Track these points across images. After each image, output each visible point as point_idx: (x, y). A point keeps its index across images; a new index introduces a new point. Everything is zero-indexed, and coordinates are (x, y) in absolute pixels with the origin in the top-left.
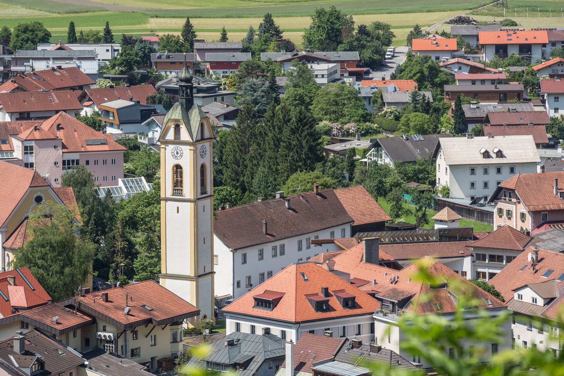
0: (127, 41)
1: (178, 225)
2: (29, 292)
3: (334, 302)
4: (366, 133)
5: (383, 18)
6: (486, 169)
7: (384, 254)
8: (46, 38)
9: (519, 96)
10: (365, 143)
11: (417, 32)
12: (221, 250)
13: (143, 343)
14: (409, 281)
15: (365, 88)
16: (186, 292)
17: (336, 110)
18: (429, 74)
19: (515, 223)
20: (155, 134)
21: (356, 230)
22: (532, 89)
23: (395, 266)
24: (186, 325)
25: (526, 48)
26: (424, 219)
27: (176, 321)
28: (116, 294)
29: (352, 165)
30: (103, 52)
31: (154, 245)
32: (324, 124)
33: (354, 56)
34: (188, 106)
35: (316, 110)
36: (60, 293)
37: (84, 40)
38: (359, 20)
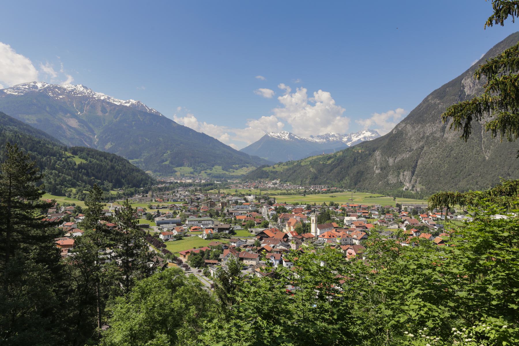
1: (313, 226)
12: (318, 229)
14: (341, 234)
15: (336, 211)
16: (314, 234)
18: (343, 209)
28: (306, 234)
30: (305, 206)
31: (310, 229)
36: (299, 234)
38: (335, 203)
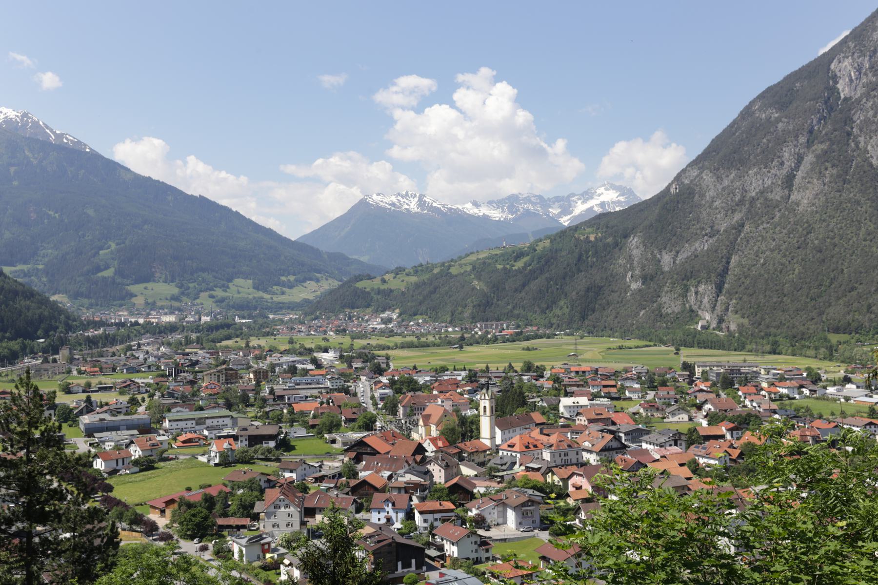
0: (470, 370)
1: (485, 424)
2: (443, 443)
3: (531, 446)
4: (539, 396)
5: (543, 363)
6: (574, 407)
7: (545, 432)
8: (447, 370)
9: (582, 386)
10: (539, 399)
11: (553, 367)
13: (475, 458)
14: (553, 439)
15: (538, 383)
16: (488, 443)
17: (530, 390)
18: (556, 379)
19: (583, 423)
20: (478, 397)
21: (537, 425)
22: (586, 384)
23: (548, 435)
24: (488, 452)
25: (584, 372)
26: (556, 421)
27: (485, 451)
28: (468, 443)
29: (535, 406)
30: (464, 374)
31: (478, 429)
32: (527, 394)
33: (535, 374)
34: (488, 389)
35: (524, 390)
36: (452, 443)
37: (458, 370)
38: (536, 364)
